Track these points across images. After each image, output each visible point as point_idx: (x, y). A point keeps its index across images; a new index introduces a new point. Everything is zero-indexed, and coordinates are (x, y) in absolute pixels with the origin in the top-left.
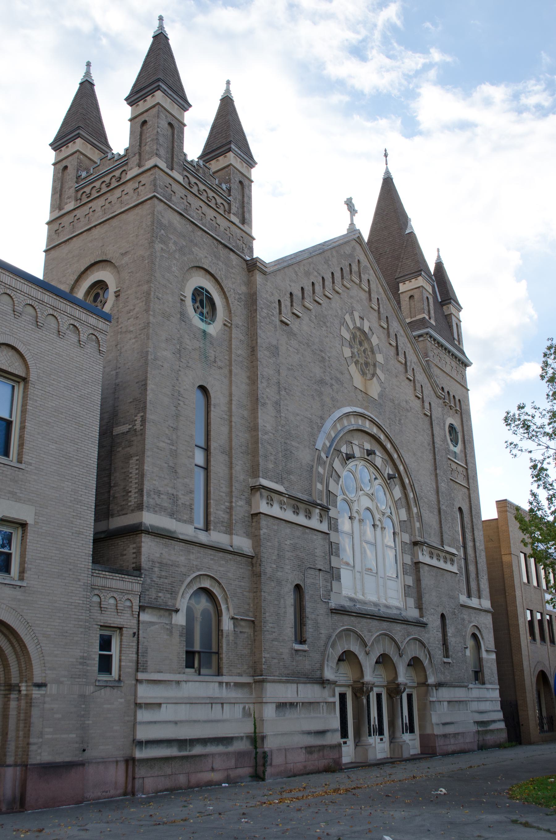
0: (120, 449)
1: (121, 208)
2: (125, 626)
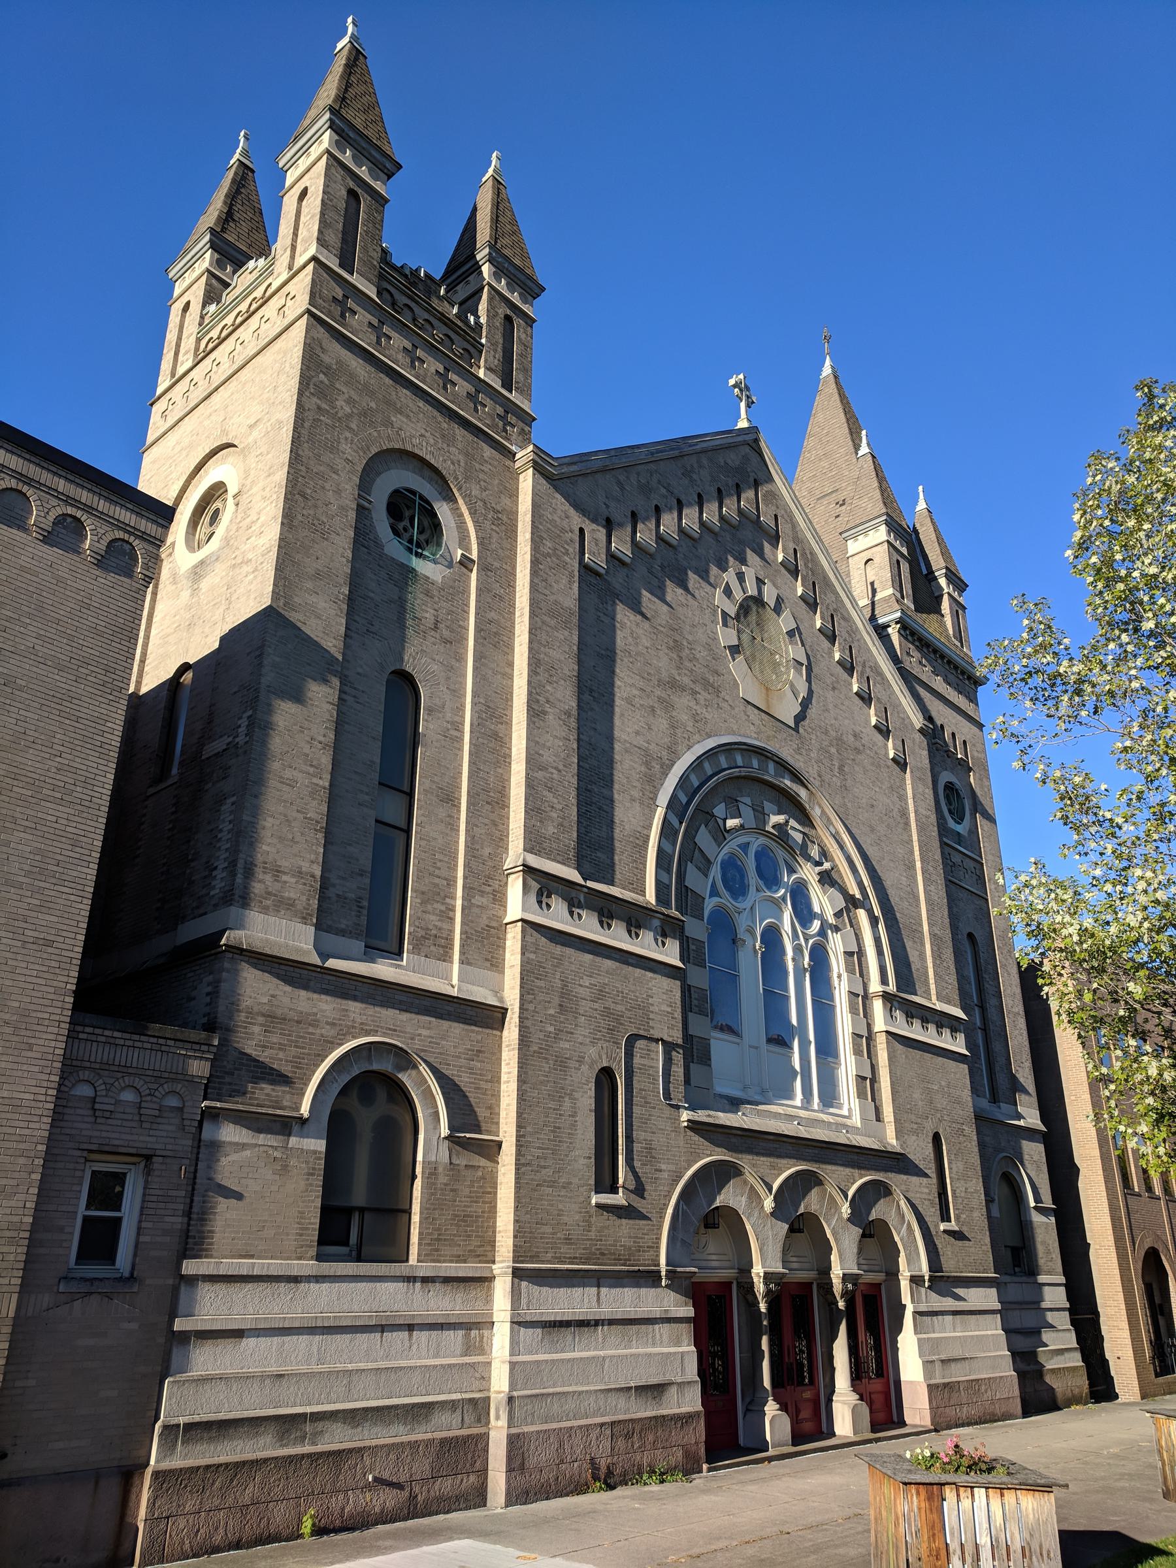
0: (210, 785)
2: (158, 1153)
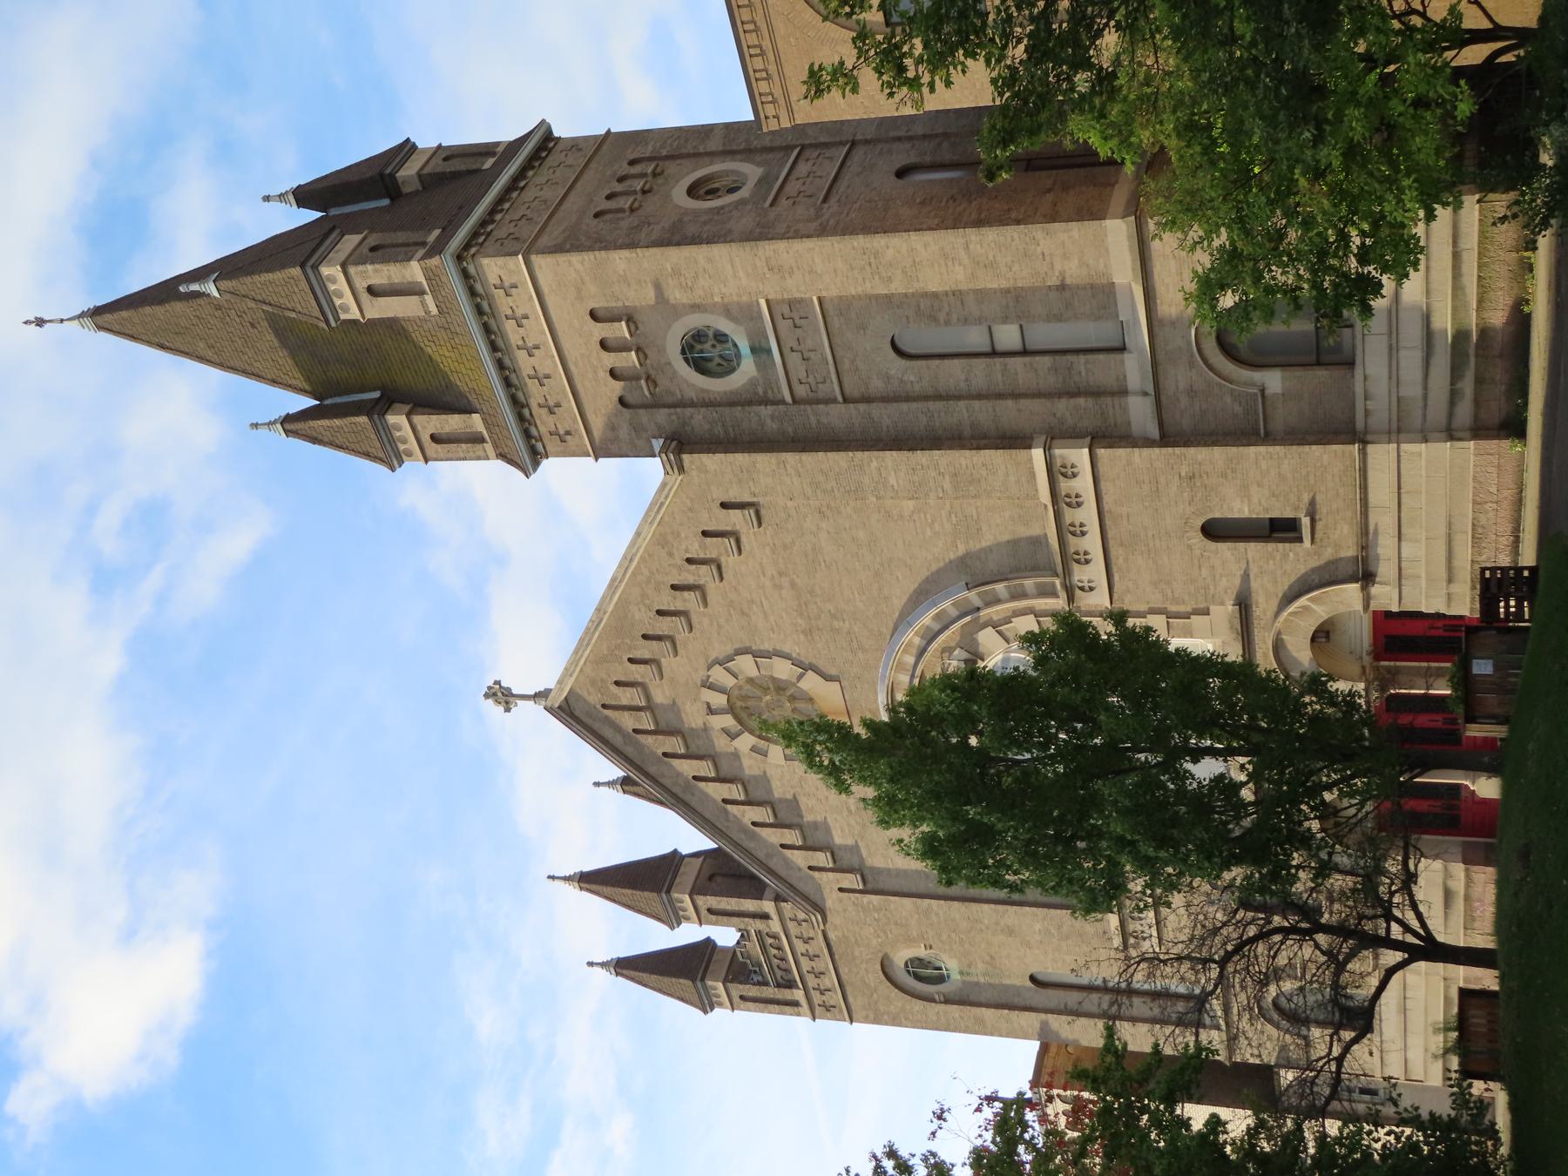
1: (537, 318)
